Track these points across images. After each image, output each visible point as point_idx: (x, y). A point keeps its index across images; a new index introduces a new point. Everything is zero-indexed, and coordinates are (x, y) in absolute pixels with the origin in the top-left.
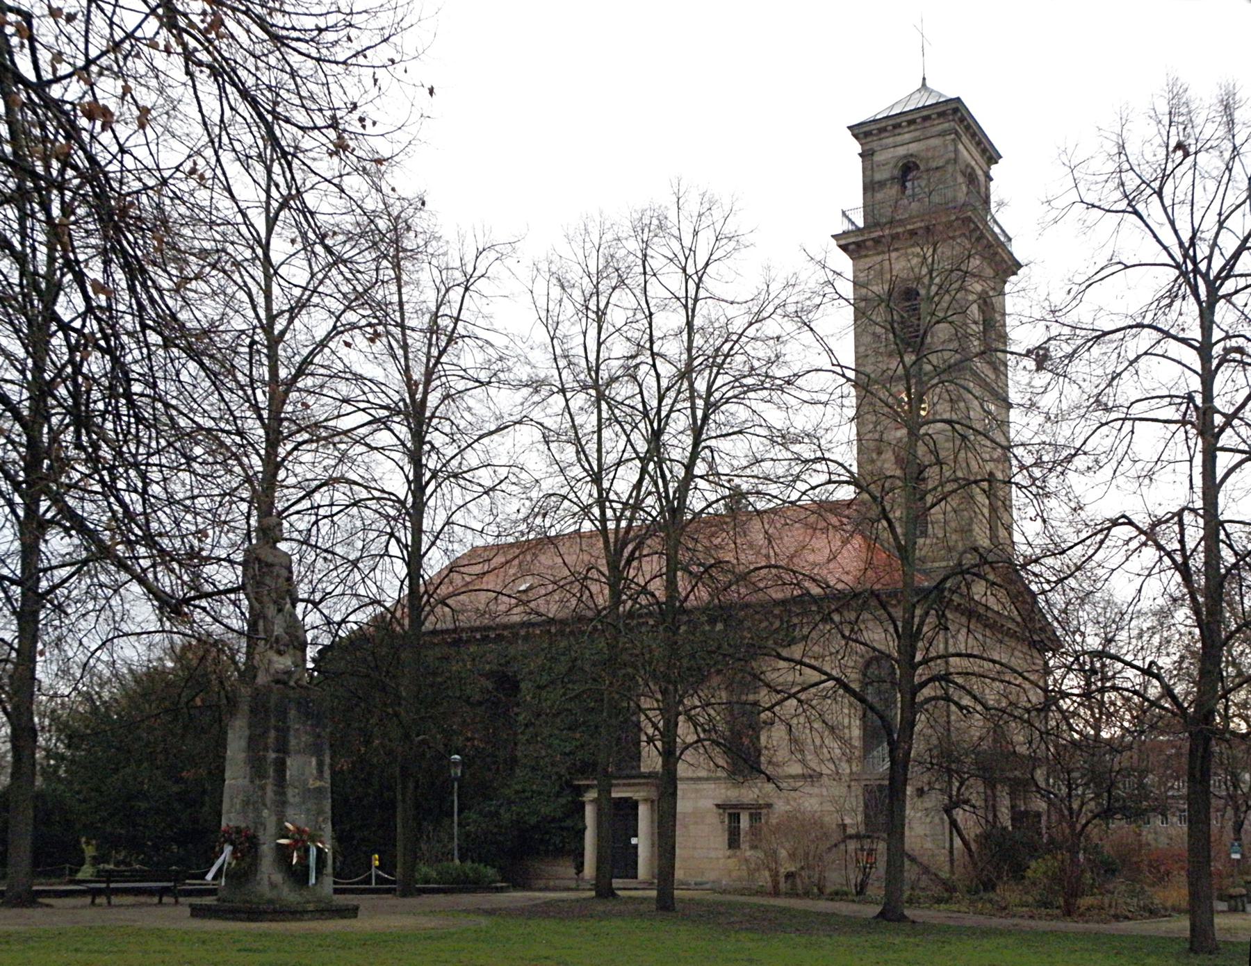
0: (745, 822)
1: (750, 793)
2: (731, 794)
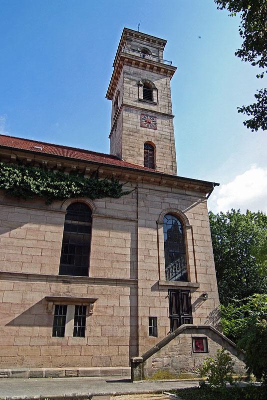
0: (71, 311)
1: (78, 290)
2: (62, 290)
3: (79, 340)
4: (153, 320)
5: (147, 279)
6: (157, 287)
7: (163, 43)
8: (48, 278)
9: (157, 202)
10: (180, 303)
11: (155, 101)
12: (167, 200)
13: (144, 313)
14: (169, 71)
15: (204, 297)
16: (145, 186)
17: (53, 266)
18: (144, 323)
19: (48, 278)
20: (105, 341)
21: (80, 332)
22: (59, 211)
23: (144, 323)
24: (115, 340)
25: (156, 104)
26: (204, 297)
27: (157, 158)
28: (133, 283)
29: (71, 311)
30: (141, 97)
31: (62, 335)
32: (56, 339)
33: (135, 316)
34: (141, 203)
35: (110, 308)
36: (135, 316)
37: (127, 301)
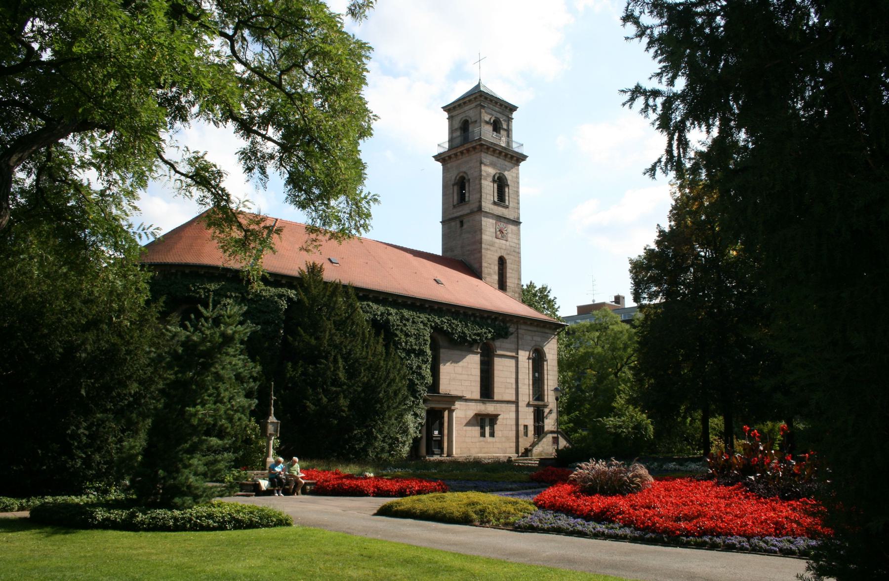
0: (487, 421)
3: (491, 439)
4: (526, 427)
5: (513, 398)
6: (528, 405)
7: (513, 108)
8: (475, 400)
9: (528, 336)
10: (539, 416)
11: (507, 203)
12: (535, 338)
13: (521, 422)
14: (518, 159)
15: (551, 412)
16: (523, 327)
17: (477, 396)
18: (521, 428)
19: (475, 400)
20: (504, 439)
21: (492, 434)
22: (477, 353)
23: (521, 428)
24: (508, 438)
25: (507, 207)
26: (551, 412)
27: (508, 275)
28: (516, 403)
29: (487, 421)
30: (496, 200)
31: (484, 436)
32: (482, 439)
33: (517, 425)
34: (520, 342)
35: (506, 416)
36: (517, 425)
37: (513, 415)
